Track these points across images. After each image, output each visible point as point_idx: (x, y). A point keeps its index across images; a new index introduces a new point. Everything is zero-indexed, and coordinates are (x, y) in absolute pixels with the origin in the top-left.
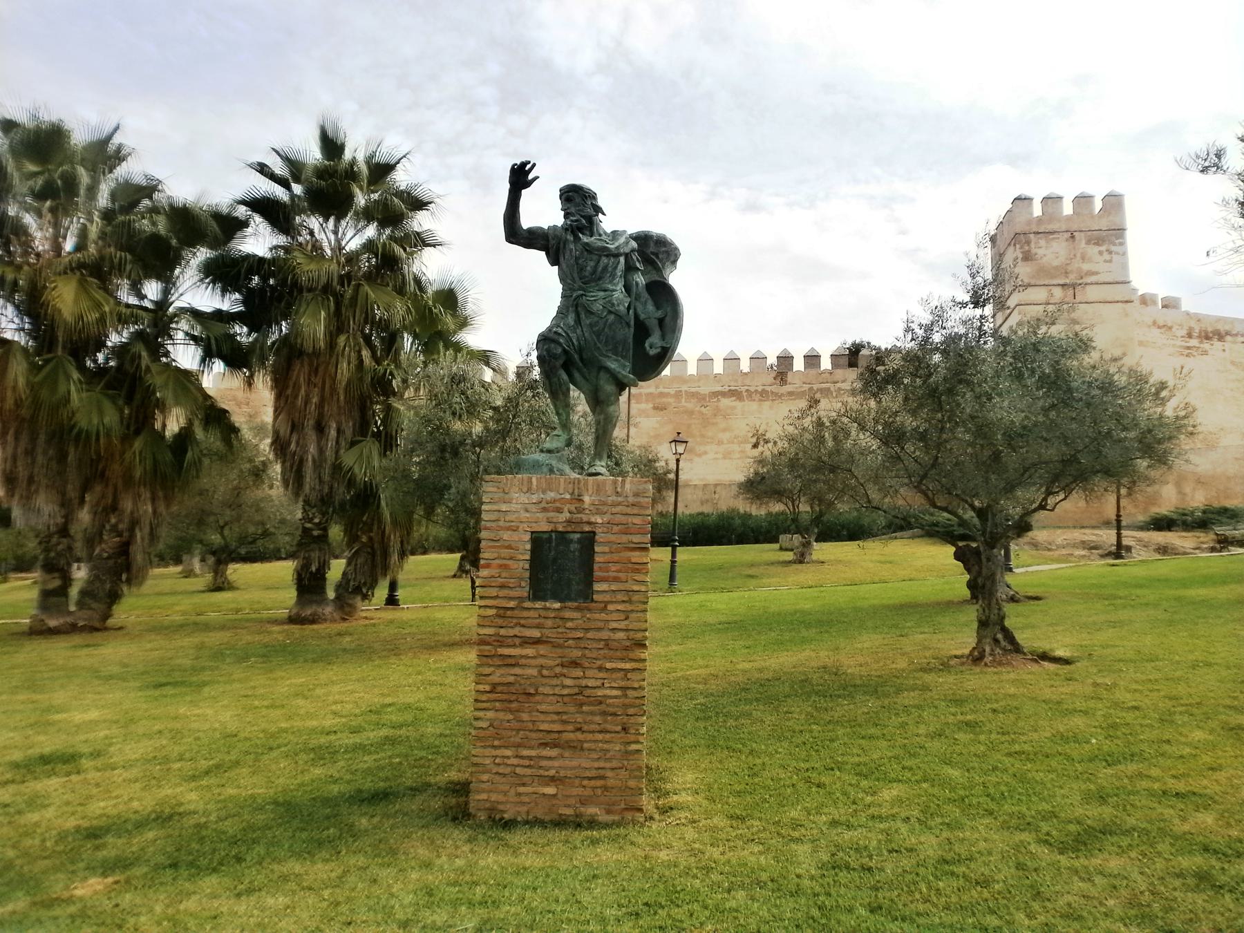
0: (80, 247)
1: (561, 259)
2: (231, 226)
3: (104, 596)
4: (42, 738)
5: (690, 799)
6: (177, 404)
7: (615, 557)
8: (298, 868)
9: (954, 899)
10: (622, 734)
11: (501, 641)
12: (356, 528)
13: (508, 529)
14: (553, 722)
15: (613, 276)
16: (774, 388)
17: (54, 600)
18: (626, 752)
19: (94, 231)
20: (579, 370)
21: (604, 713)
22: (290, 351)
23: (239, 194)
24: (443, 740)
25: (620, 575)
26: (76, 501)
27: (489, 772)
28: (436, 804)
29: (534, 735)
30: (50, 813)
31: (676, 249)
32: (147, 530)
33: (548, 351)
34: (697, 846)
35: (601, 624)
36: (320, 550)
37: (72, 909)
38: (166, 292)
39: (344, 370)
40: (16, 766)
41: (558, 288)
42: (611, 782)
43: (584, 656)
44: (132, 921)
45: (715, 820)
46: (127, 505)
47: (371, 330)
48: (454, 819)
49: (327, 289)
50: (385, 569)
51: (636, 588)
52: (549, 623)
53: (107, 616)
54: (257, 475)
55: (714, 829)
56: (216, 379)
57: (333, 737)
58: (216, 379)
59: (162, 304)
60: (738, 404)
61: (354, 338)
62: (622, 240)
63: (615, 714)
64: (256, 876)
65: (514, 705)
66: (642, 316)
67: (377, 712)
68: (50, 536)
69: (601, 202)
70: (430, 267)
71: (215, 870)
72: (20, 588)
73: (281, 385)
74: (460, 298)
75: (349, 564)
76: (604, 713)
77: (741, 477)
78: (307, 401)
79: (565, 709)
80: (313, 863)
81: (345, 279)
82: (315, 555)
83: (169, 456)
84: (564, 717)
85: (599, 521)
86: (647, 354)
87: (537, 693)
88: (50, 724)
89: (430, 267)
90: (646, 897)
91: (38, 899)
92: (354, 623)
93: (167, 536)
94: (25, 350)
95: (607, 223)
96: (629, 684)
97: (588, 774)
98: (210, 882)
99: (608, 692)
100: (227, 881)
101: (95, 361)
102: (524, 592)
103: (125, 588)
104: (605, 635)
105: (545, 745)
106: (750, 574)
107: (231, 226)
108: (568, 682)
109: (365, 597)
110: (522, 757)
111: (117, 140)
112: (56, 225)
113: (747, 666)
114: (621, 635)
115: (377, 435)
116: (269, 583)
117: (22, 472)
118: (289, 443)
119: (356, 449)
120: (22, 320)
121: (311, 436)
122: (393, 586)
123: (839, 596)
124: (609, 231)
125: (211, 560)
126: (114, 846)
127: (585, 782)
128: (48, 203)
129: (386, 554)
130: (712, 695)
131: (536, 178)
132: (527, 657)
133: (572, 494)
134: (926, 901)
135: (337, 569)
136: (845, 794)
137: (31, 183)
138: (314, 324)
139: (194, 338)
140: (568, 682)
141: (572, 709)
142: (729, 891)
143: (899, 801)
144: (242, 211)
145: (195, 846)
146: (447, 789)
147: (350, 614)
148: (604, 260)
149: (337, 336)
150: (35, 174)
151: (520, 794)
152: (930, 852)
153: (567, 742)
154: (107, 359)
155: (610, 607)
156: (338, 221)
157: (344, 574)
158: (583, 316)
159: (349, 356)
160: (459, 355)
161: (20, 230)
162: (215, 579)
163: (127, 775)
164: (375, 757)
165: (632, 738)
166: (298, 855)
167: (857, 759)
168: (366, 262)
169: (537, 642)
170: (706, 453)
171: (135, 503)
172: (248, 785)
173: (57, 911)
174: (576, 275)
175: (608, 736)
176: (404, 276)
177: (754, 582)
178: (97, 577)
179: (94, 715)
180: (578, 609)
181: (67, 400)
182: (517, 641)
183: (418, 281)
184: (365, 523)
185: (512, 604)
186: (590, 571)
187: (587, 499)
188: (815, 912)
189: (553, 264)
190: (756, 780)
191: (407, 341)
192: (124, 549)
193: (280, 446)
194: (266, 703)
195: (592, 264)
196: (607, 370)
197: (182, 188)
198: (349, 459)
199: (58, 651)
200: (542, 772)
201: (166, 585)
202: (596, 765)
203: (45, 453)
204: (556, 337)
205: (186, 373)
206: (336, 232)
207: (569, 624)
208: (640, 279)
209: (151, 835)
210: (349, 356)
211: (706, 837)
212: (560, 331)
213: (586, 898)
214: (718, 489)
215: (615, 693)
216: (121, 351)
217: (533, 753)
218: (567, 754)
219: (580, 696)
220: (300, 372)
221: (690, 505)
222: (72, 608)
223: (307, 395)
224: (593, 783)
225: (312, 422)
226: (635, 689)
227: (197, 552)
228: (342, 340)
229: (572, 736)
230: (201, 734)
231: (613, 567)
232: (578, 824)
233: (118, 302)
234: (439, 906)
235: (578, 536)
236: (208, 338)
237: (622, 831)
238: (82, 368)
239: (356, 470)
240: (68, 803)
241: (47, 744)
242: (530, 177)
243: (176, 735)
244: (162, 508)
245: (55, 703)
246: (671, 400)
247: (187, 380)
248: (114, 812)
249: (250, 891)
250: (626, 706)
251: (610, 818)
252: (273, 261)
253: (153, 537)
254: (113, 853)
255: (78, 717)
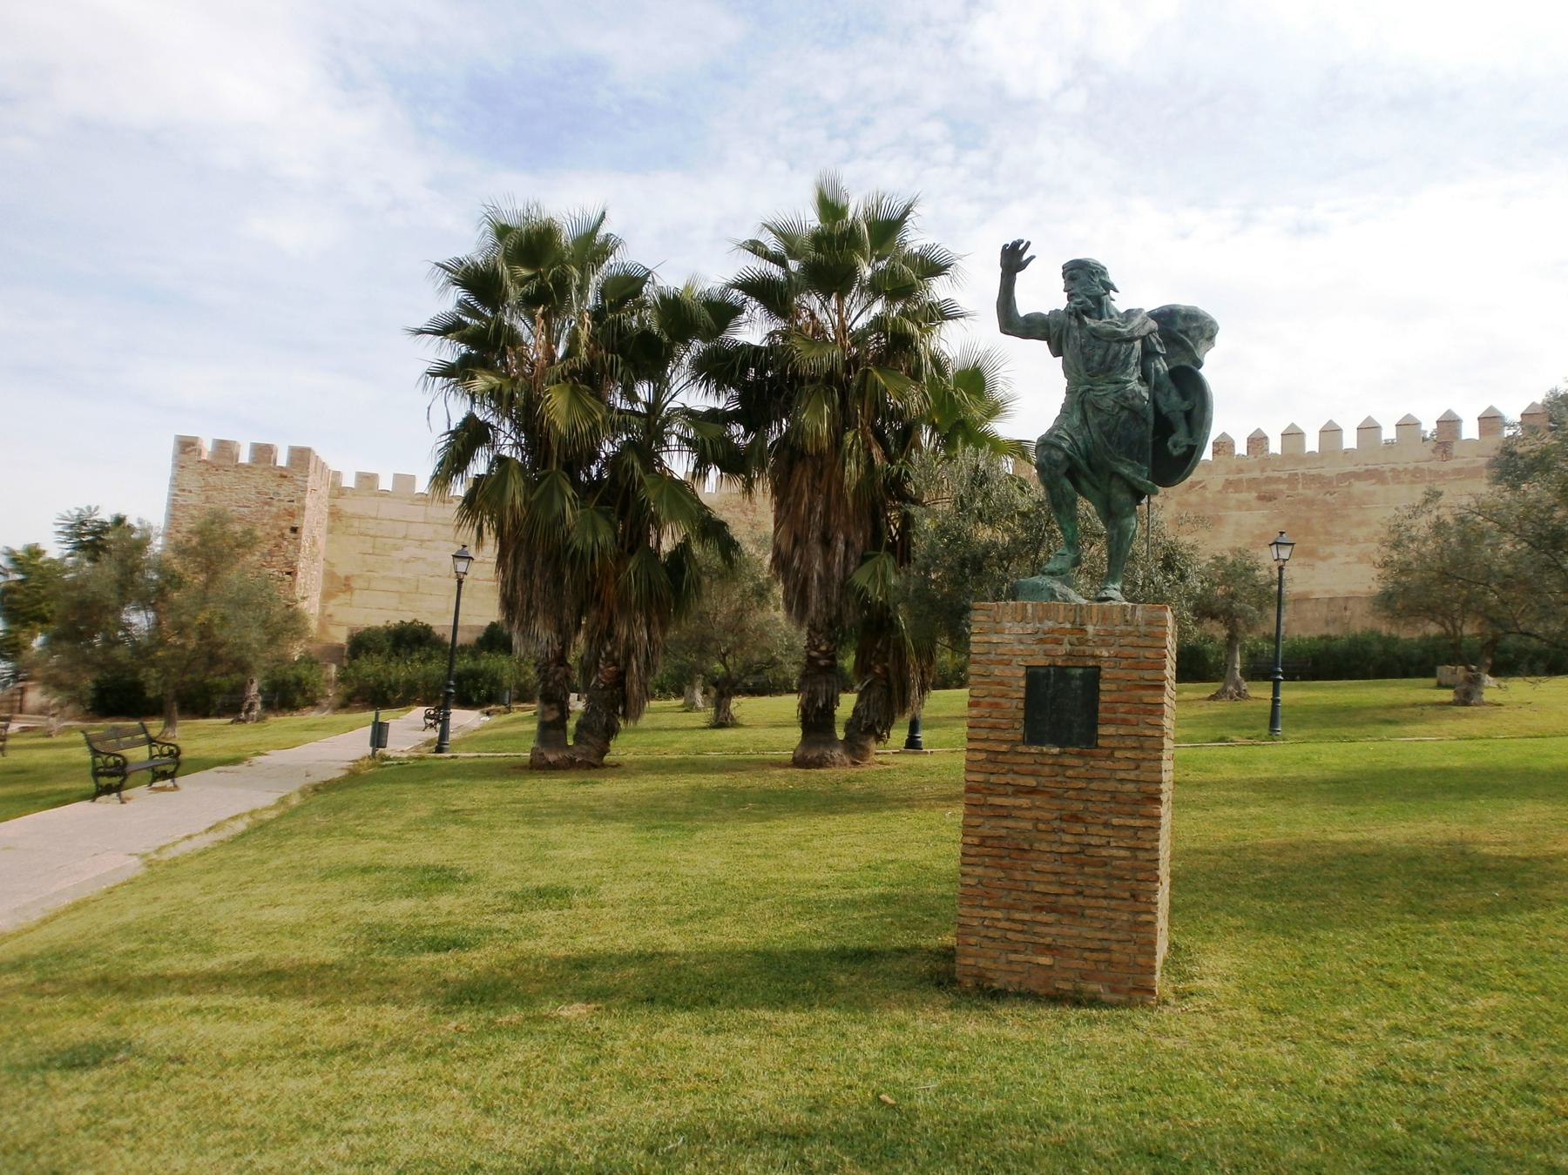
0: (569, 354)
1: (1065, 349)
2: (723, 313)
3: (600, 730)
4: (538, 872)
5: (1217, 985)
6: (672, 518)
7: (1124, 696)
8: (768, 1015)
9: (1524, 1129)
10: (1131, 902)
11: (991, 790)
12: (868, 661)
13: (1000, 662)
14: (1050, 883)
15: (1126, 364)
16: (1434, 465)
17: (552, 732)
18: (1135, 923)
19: (584, 334)
20: (1085, 476)
21: (1109, 877)
22: (791, 454)
23: (731, 275)
24: (943, 901)
25: (1129, 717)
26: (572, 627)
27: (977, 934)
28: (923, 968)
29: (1028, 897)
30: (543, 942)
31: (1212, 322)
32: (642, 659)
33: (1048, 458)
34: (1211, 1037)
35: (1106, 774)
36: (828, 682)
37: (558, 1027)
38: (658, 394)
39: (853, 470)
40: (515, 896)
41: (1063, 382)
42: (1116, 957)
43: (1086, 809)
44: (610, 1043)
45: (1242, 1012)
46: (622, 631)
47: (883, 423)
48: (939, 984)
49: (831, 378)
50: (904, 704)
51: (1148, 732)
52: (1047, 770)
53: (604, 751)
54: (761, 595)
55: (1239, 1020)
56: (714, 488)
57: (824, 892)
58: (714, 488)
59: (654, 407)
60: (1379, 488)
61: (864, 435)
62: (1137, 321)
63: (1122, 879)
64: (724, 1015)
65: (1006, 861)
66: (1165, 410)
67: (876, 869)
68: (548, 664)
69: (1113, 278)
70: (949, 344)
71: (689, 1008)
72: (523, 720)
73: (781, 492)
74: (988, 378)
75: (860, 699)
76: (1109, 877)
77: (1377, 588)
78: (811, 510)
79: (1064, 869)
80: (785, 1012)
81: (852, 363)
82: (822, 688)
83: (664, 577)
84: (1063, 878)
85: (1105, 654)
86: (1169, 455)
87: (1032, 849)
88: (545, 859)
89: (949, 344)
90: (1135, 1082)
91: (531, 1014)
92: (866, 770)
93: (663, 668)
94: (521, 467)
95: (1120, 302)
96: (1139, 844)
97: (1089, 945)
98: (682, 1018)
99: (1115, 852)
100: (699, 1019)
101: (589, 475)
102: (1019, 734)
103: (622, 723)
104: (1111, 786)
105: (1040, 909)
106: (1390, 716)
107: (723, 313)
108: (1068, 838)
109: (879, 738)
110: (1014, 921)
111: (602, 232)
112: (549, 330)
113: (1342, 837)
114: (1130, 787)
115: (891, 548)
116: (771, 720)
117: (521, 597)
118: (792, 559)
119: (868, 566)
120: (518, 435)
121: (818, 550)
122: (914, 726)
123: (1507, 753)
124: (1122, 310)
125: (713, 692)
126: (598, 978)
127: (1086, 954)
128: (541, 310)
129: (904, 689)
130: (1283, 869)
131: (1032, 258)
132: (1020, 808)
133: (1073, 623)
134: (1486, 1126)
135: (847, 704)
136: (1424, 999)
137: (525, 289)
138: (818, 420)
139: (689, 442)
140: (1068, 838)
141: (1072, 870)
142: (1236, 1088)
143: (1494, 1013)
144: (736, 295)
145: (673, 985)
146: (938, 953)
147: (862, 758)
148: (1115, 347)
149: (844, 432)
150: (527, 280)
151: (1010, 962)
152: (1514, 1075)
153: (1066, 906)
154: (599, 472)
155: (1118, 754)
156: (841, 299)
157: (856, 710)
158: (1090, 414)
159: (858, 456)
160: (981, 451)
161: (514, 339)
162: (717, 715)
163: (614, 914)
164: (865, 914)
165: (1142, 907)
166: (771, 1004)
167: (1455, 958)
168: (874, 343)
169: (1032, 791)
170: (1332, 555)
171: (630, 629)
172: (730, 934)
173: (546, 1027)
174: (1081, 367)
175: (1113, 903)
176: (918, 355)
177: (1392, 729)
178: (593, 709)
179: (587, 853)
180: (1080, 755)
181: (562, 517)
182: (1010, 790)
183: (936, 362)
184: (879, 651)
185: (1004, 748)
186: (1095, 712)
187: (1090, 629)
188: (1334, 1120)
189: (1055, 355)
190: (1310, 972)
191: (925, 436)
192: (620, 680)
193: (781, 562)
194: (758, 852)
195: (1100, 352)
196: (1120, 476)
197: (669, 278)
198: (861, 578)
199: (557, 788)
200: (1036, 939)
201: (666, 720)
202: (1100, 935)
203: (541, 576)
204: (1057, 441)
205: (680, 483)
206: (839, 313)
207: (1070, 773)
208: (1162, 366)
209: (632, 971)
210: (858, 456)
211: (1226, 1030)
212: (1062, 433)
213: (1066, 1076)
214: (1351, 604)
215: (1123, 853)
216: (613, 462)
217: (1026, 917)
218: (1065, 921)
219: (1081, 856)
220: (803, 477)
221: (1301, 627)
222: (570, 742)
223: (811, 502)
224: (1095, 956)
225: (816, 534)
226: (1146, 850)
227: (699, 682)
228: (849, 437)
229: (1071, 900)
230: (689, 880)
231: (1122, 708)
232: (1077, 1000)
233: (611, 408)
234: (905, 1065)
235: (1080, 671)
236: (703, 441)
237: (1128, 1012)
238: (575, 483)
239: (871, 590)
240: (559, 935)
241: (543, 878)
242: (1025, 257)
243: (663, 878)
244: (657, 635)
245: (553, 839)
246: (1283, 487)
247: (681, 493)
248: (601, 947)
249: (718, 1031)
250: (1134, 869)
251: (1115, 997)
252: (772, 349)
253: (649, 667)
254: (597, 984)
255: (572, 855)
